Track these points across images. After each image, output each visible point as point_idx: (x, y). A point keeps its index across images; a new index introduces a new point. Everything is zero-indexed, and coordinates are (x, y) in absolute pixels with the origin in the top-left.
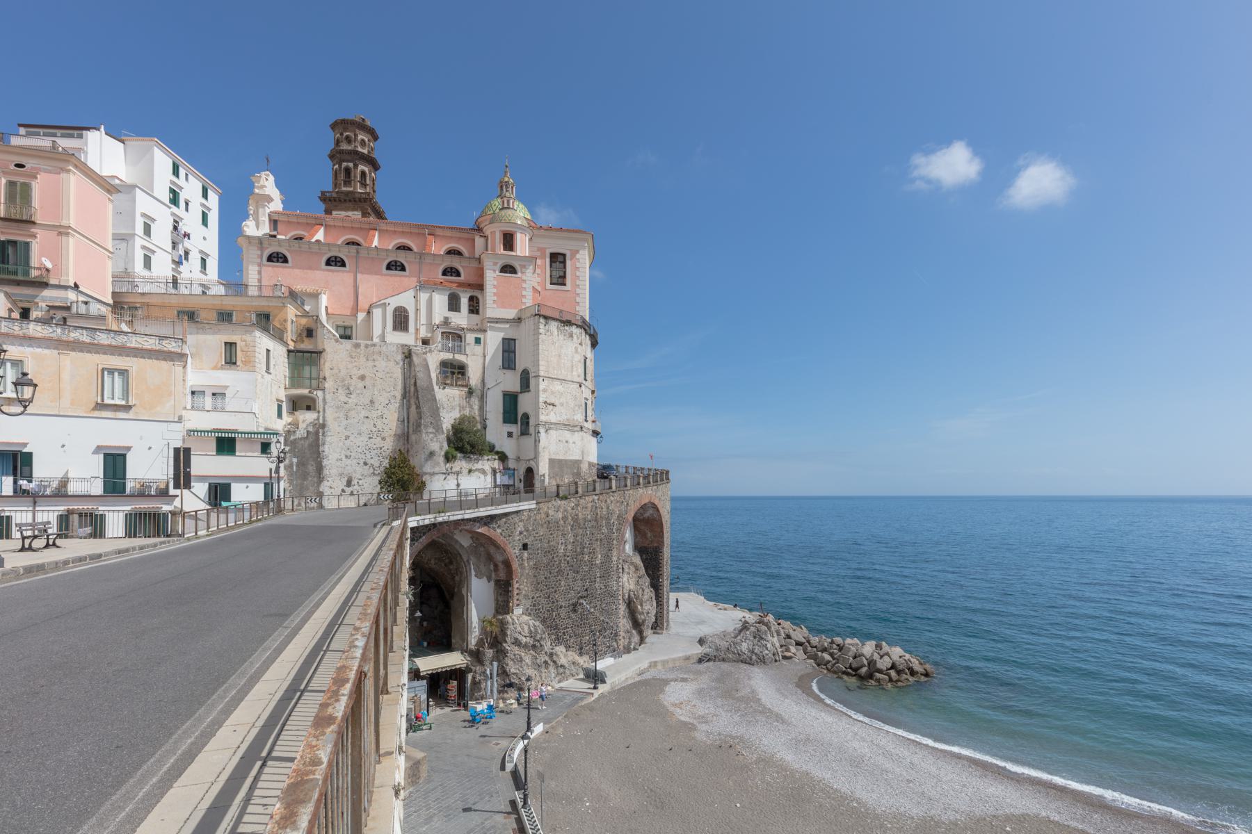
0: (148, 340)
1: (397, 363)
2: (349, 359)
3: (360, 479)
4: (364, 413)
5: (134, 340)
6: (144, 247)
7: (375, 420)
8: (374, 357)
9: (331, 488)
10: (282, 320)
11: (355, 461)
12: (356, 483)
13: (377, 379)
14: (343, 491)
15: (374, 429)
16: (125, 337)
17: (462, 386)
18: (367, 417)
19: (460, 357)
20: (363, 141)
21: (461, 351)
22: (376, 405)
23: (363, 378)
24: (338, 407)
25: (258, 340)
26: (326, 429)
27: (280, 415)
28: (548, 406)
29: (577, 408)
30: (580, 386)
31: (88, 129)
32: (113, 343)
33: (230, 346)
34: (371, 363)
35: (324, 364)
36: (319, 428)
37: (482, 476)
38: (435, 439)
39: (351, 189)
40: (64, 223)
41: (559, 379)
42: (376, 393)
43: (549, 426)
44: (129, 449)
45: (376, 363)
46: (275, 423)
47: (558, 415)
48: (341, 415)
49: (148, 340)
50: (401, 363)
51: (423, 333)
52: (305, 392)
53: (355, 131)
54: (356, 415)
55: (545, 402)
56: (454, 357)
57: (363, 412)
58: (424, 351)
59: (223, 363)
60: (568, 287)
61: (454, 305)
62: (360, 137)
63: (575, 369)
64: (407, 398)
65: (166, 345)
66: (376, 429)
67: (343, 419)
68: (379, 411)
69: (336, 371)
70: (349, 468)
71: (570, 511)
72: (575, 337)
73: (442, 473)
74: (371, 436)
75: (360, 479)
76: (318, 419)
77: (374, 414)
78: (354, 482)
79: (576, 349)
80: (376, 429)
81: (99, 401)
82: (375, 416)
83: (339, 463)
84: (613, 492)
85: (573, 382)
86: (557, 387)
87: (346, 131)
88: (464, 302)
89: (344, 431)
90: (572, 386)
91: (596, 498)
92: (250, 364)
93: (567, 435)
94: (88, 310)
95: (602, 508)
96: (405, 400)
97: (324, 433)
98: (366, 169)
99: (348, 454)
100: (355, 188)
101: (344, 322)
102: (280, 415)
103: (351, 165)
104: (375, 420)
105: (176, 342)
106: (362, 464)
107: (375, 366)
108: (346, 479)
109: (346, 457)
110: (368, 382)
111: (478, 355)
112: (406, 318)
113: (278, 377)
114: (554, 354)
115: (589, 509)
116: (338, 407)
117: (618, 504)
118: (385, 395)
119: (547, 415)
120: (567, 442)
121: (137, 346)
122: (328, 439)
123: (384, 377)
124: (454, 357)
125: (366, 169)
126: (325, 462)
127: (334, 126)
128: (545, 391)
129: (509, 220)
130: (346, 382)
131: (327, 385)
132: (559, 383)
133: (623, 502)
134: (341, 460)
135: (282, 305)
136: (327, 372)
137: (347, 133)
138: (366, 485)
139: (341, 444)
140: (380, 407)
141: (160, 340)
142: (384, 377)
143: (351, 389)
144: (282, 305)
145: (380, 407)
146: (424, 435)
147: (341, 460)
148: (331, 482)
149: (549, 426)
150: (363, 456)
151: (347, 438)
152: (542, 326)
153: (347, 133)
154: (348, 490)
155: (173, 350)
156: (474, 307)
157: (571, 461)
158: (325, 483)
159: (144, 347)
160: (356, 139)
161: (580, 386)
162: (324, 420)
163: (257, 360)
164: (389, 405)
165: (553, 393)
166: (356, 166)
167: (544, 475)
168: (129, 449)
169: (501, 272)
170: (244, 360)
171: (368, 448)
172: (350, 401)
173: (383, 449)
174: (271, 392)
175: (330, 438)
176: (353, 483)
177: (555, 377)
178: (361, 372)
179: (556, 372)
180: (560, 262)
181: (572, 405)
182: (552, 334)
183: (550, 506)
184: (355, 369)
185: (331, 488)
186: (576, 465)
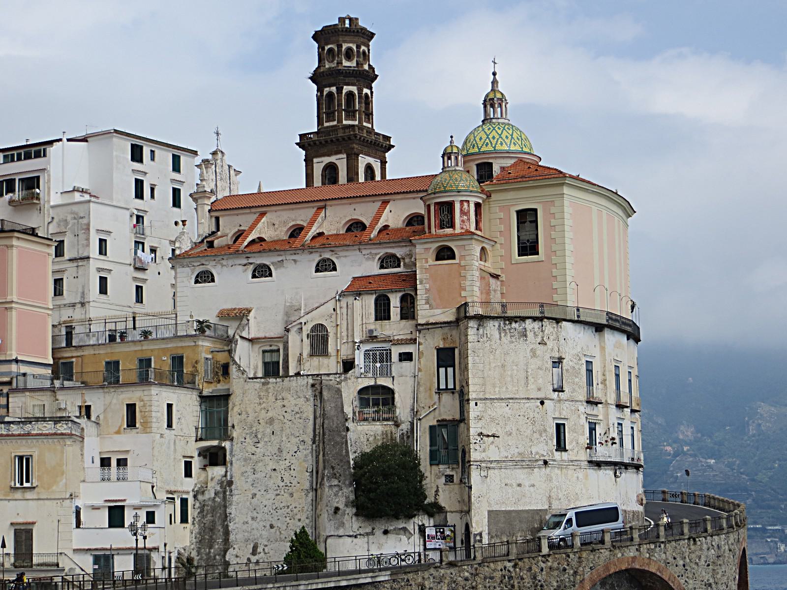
0: (46, 425)
1: (308, 400)
2: (257, 401)
3: (266, 546)
4: (272, 465)
5: (36, 427)
6: (99, 270)
7: (283, 472)
8: (283, 394)
9: (237, 556)
10: (194, 361)
11: (262, 523)
12: (262, 551)
13: (285, 421)
14: (249, 559)
15: (282, 484)
16: (30, 426)
17: (387, 420)
18: (275, 470)
19: (383, 381)
20: (349, 50)
21: (386, 372)
22: (285, 453)
23: (271, 421)
24: (245, 460)
25: (155, 398)
26: (233, 487)
27: (188, 473)
28: (485, 438)
29: (536, 435)
30: (542, 403)
31: (50, 143)
32: (22, 433)
33: (131, 408)
34: (279, 403)
35: (232, 409)
36: (227, 484)
37: (404, 538)
38: (340, 494)
39: (335, 123)
40: (9, 299)
41: (502, 399)
42: (284, 439)
43: (487, 465)
44: (33, 523)
45: (285, 402)
46: (182, 484)
47: (502, 449)
48: (249, 469)
49: (46, 425)
50: (312, 399)
51: (345, 353)
52: (215, 443)
53: (338, 41)
54: (264, 467)
55: (481, 434)
56: (376, 382)
57: (271, 463)
58: (338, 380)
59: (125, 426)
60: (542, 255)
61: (382, 312)
62: (345, 46)
63: (531, 380)
64: (317, 443)
65: (60, 428)
66: (283, 484)
67: (249, 473)
68: (287, 461)
69: (244, 416)
70: (255, 532)
71: (462, 583)
72: (530, 335)
73: (348, 536)
74: (278, 492)
75: (266, 546)
76: (226, 476)
77: (283, 465)
78: (260, 550)
79: (533, 351)
80: (283, 484)
81: (13, 485)
82: (283, 467)
83: (245, 527)
84: (543, 556)
85: (528, 399)
86: (501, 409)
87: (327, 44)
88: (395, 301)
89: (251, 487)
90: (527, 405)
91: (509, 565)
92: (147, 426)
93: (520, 475)
94: (25, 382)
95: (522, 579)
96: (314, 446)
97: (231, 491)
98: (354, 89)
99: (255, 514)
100: (340, 121)
101: (271, 346)
102: (188, 473)
103: (334, 89)
104: (283, 472)
105: (67, 424)
106: (268, 527)
107: (284, 406)
108: (252, 546)
109: (253, 519)
110: (276, 427)
111: (407, 376)
112: (325, 340)
113: (184, 431)
114: (493, 365)
115: (498, 581)
116: (245, 460)
117: (556, 573)
118: (294, 440)
119: (484, 451)
120: (519, 485)
121: (38, 432)
122: (235, 498)
123: (293, 418)
124: (376, 382)
125: (354, 89)
126: (231, 526)
127: (316, 37)
128: (479, 418)
129: (445, 187)
130: (254, 429)
131: (235, 435)
132: (504, 405)
133: (565, 570)
134: (247, 523)
135: (193, 344)
136: (233, 418)
137: (329, 46)
138: (272, 553)
139: (248, 503)
140: (288, 457)
141: (55, 424)
142: (293, 418)
143: (259, 436)
144: (193, 344)
145: (288, 457)
146: (327, 489)
147: (247, 523)
148: (237, 549)
149: (487, 465)
150: (269, 517)
151: (254, 495)
152: (471, 332)
153: (329, 46)
154: (254, 559)
155: (64, 432)
156: (408, 312)
157: (527, 511)
158: (231, 551)
159: (44, 432)
160: (340, 51)
161: (542, 403)
162: (231, 478)
163: (154, 420)
164: (298, 453)
165: (493, 420)
166: (340, 90)
167: (480, 534)
168: (33, 523)
169: (438, 259)
170: (142, 421)
171: (274, 508)
172: (258, 450)
173: (290, 507)
174: (175, 450)
175: (237, 497)
176: (259, 550)
177: (497, 397)
178: (270, 414)
179: (497, 389)
180: (531, 222)
181: (529, 432)
182: (490, 339)
183: (426, 577)
184: (263, 411)
185: (237, 556)
186: (537, 518)
